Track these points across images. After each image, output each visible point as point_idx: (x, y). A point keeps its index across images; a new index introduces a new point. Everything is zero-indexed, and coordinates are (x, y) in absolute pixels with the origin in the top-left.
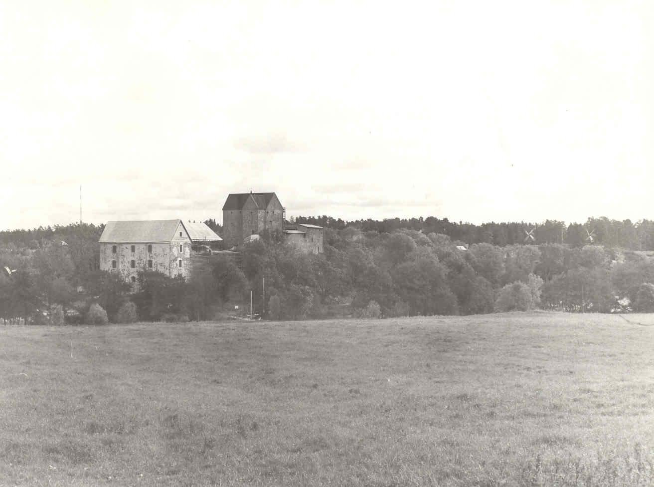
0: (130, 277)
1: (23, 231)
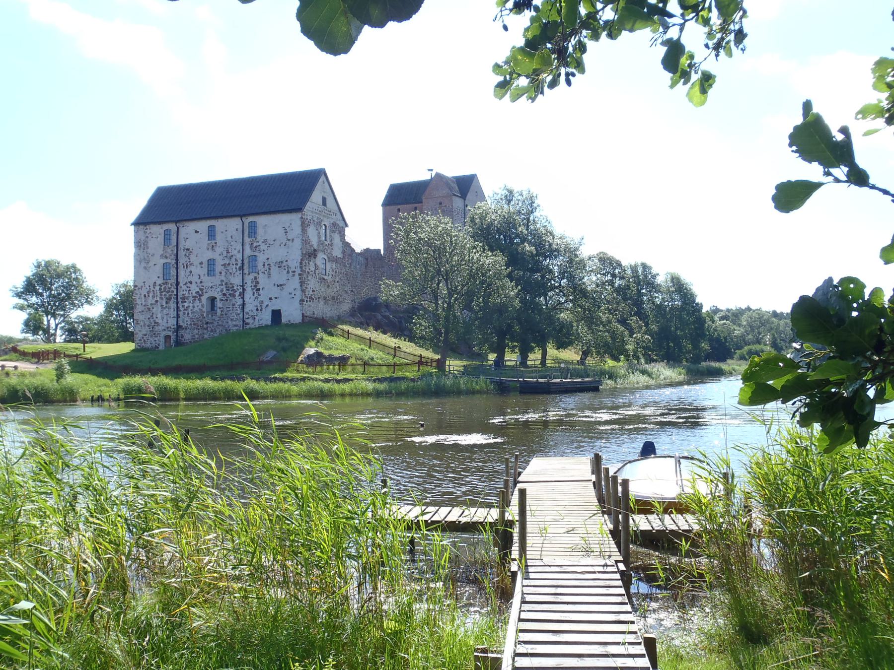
0: (204, 299)
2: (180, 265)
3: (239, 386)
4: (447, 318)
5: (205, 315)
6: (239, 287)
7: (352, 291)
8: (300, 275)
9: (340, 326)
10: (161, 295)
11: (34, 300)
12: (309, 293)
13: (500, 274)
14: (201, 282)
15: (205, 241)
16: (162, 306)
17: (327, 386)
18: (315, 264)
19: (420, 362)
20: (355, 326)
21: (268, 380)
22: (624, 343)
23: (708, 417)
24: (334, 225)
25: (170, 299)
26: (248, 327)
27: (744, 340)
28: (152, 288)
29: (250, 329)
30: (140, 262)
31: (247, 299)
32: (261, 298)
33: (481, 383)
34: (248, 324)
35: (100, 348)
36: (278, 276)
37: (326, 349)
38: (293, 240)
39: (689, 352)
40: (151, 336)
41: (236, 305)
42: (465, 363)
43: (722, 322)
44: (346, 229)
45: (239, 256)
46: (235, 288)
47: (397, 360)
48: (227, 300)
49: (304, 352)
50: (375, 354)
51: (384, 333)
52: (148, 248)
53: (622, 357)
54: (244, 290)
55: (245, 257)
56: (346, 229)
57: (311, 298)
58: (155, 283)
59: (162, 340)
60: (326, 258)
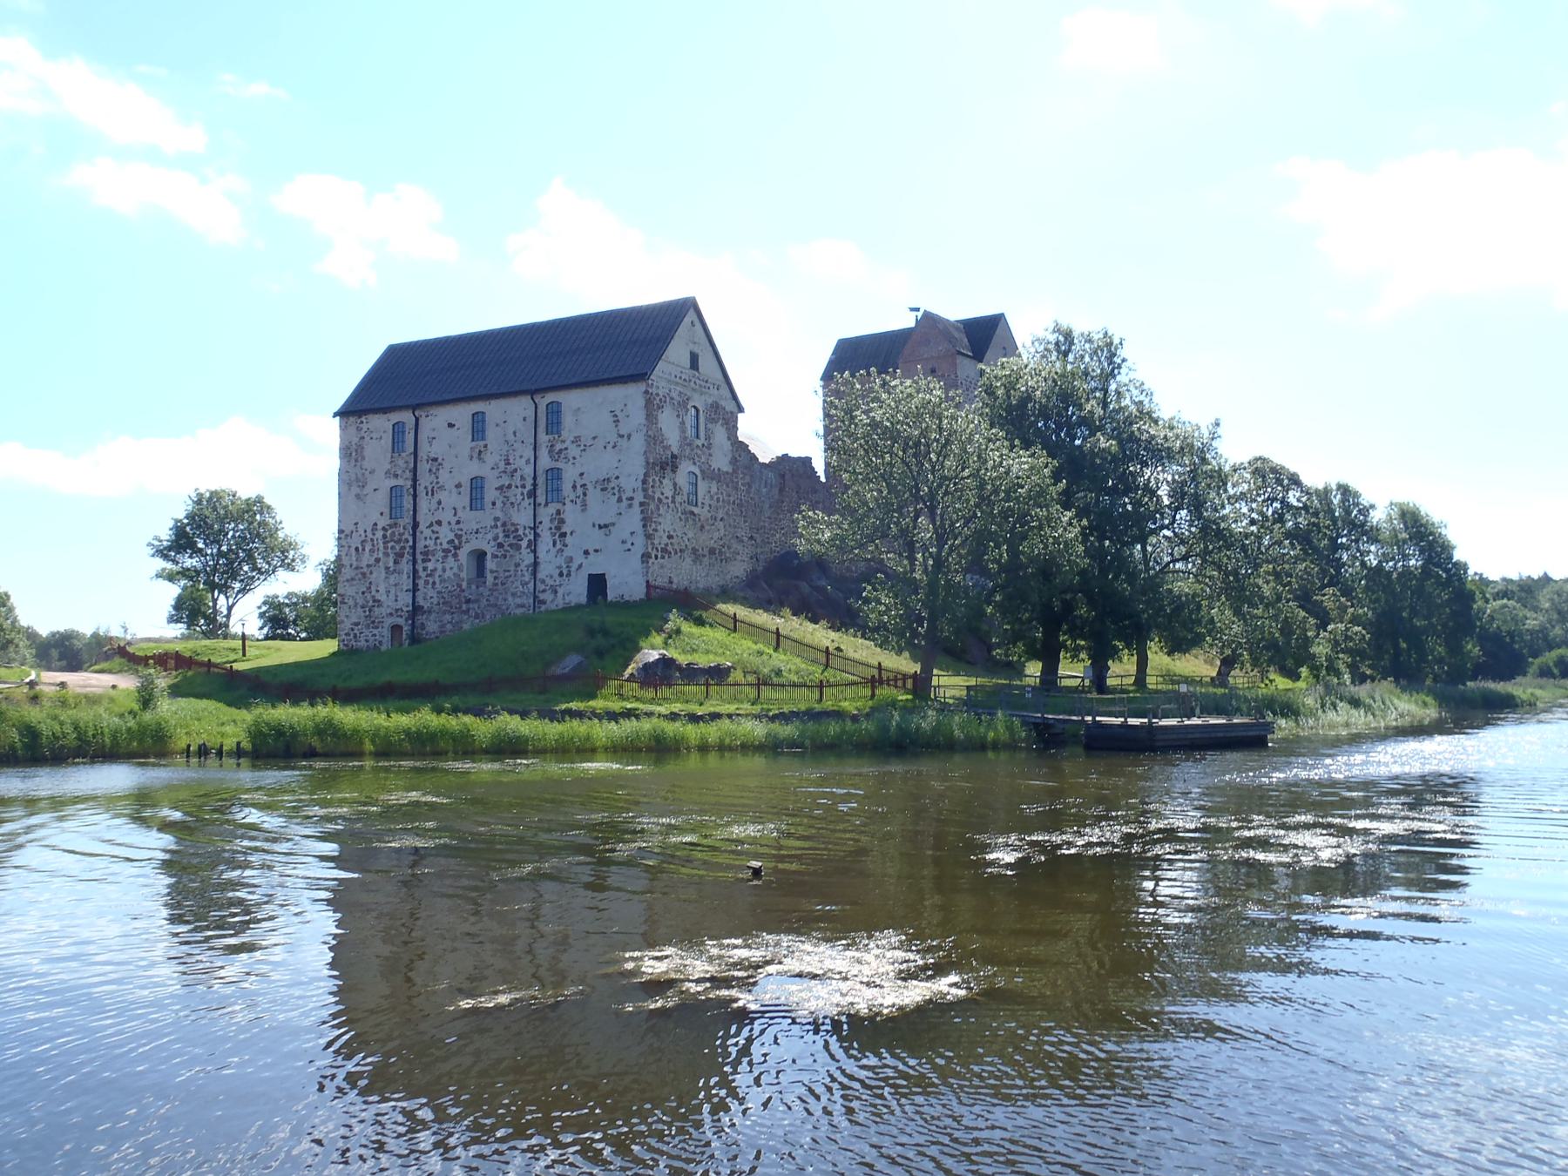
2: (421, 489)
3: (482, 728)
4: (932, 586)
5: (464, 585)
6: (527, 531)
7: (751, 538)
8: (641, 504)
9: (722, 607)
10: (386, 548)
11: (190, 562)
12: (661, 539)
13: (1042, 493)
14: (458, 522)
15: (466, 444)
16: (387, 568)
17: (671, 728)
18: (675, 485)
19: (877, 679)
20: (754, 606)
21: (553, 716)
22: (1307, 642)
23: (1488, 795)
24: (715, 407)
25: (402, 556)
26: (543, 608)
27: (1545, 638)
28: (370, 535)
29: (547, 611)
30: (350, 485)
31: (542, 554)
32: (568, 552)
33: (1000, 725)
34: (543, 602)
35: (278, 650)
36: (597, 502)
37: (684, 652)
38: (629, 436)
39: (1440, 661)
40: (368, 626)
41: (523, 566)
42: (972, 682)
43: (1500, 602)
44: (740, 415)
45: (529, 470)
46: (520, 532)
47: (830, 675)
48: (505, 557)
49: (638, 657)
50: (787, 663)
51: (815, 621)
52: (363, 458)
53: (1304, 671)
54: (536, 535)
55: (540, 472)
56: (740, 415)
57: (664, 550)
58: (375, 524)
59: (386, 633)
60: (697, 471)
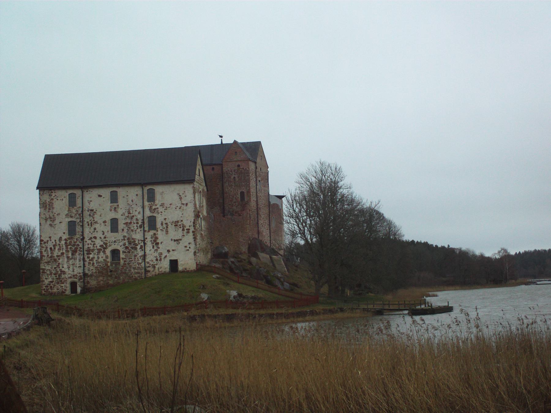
1: (545, 251)
